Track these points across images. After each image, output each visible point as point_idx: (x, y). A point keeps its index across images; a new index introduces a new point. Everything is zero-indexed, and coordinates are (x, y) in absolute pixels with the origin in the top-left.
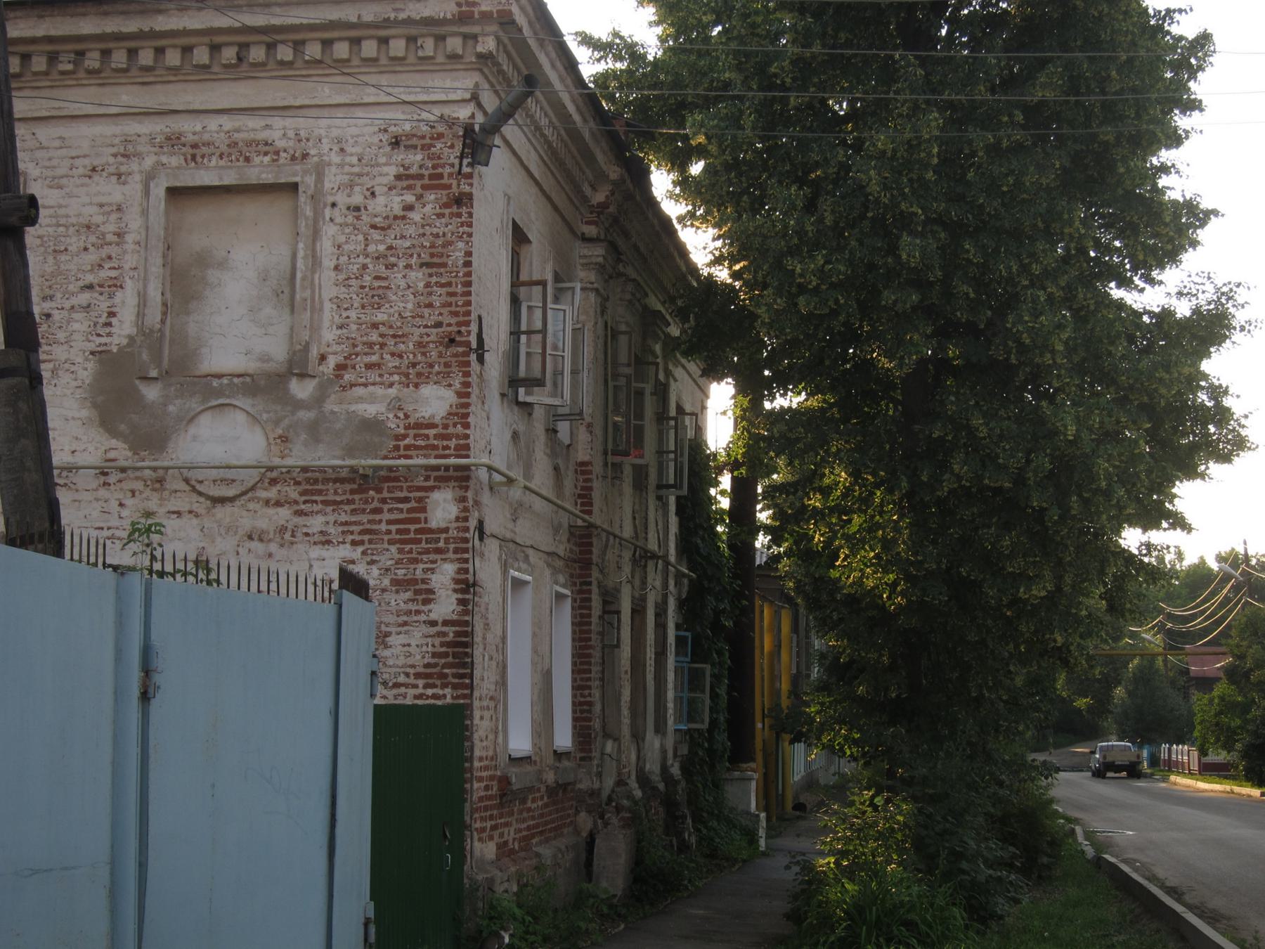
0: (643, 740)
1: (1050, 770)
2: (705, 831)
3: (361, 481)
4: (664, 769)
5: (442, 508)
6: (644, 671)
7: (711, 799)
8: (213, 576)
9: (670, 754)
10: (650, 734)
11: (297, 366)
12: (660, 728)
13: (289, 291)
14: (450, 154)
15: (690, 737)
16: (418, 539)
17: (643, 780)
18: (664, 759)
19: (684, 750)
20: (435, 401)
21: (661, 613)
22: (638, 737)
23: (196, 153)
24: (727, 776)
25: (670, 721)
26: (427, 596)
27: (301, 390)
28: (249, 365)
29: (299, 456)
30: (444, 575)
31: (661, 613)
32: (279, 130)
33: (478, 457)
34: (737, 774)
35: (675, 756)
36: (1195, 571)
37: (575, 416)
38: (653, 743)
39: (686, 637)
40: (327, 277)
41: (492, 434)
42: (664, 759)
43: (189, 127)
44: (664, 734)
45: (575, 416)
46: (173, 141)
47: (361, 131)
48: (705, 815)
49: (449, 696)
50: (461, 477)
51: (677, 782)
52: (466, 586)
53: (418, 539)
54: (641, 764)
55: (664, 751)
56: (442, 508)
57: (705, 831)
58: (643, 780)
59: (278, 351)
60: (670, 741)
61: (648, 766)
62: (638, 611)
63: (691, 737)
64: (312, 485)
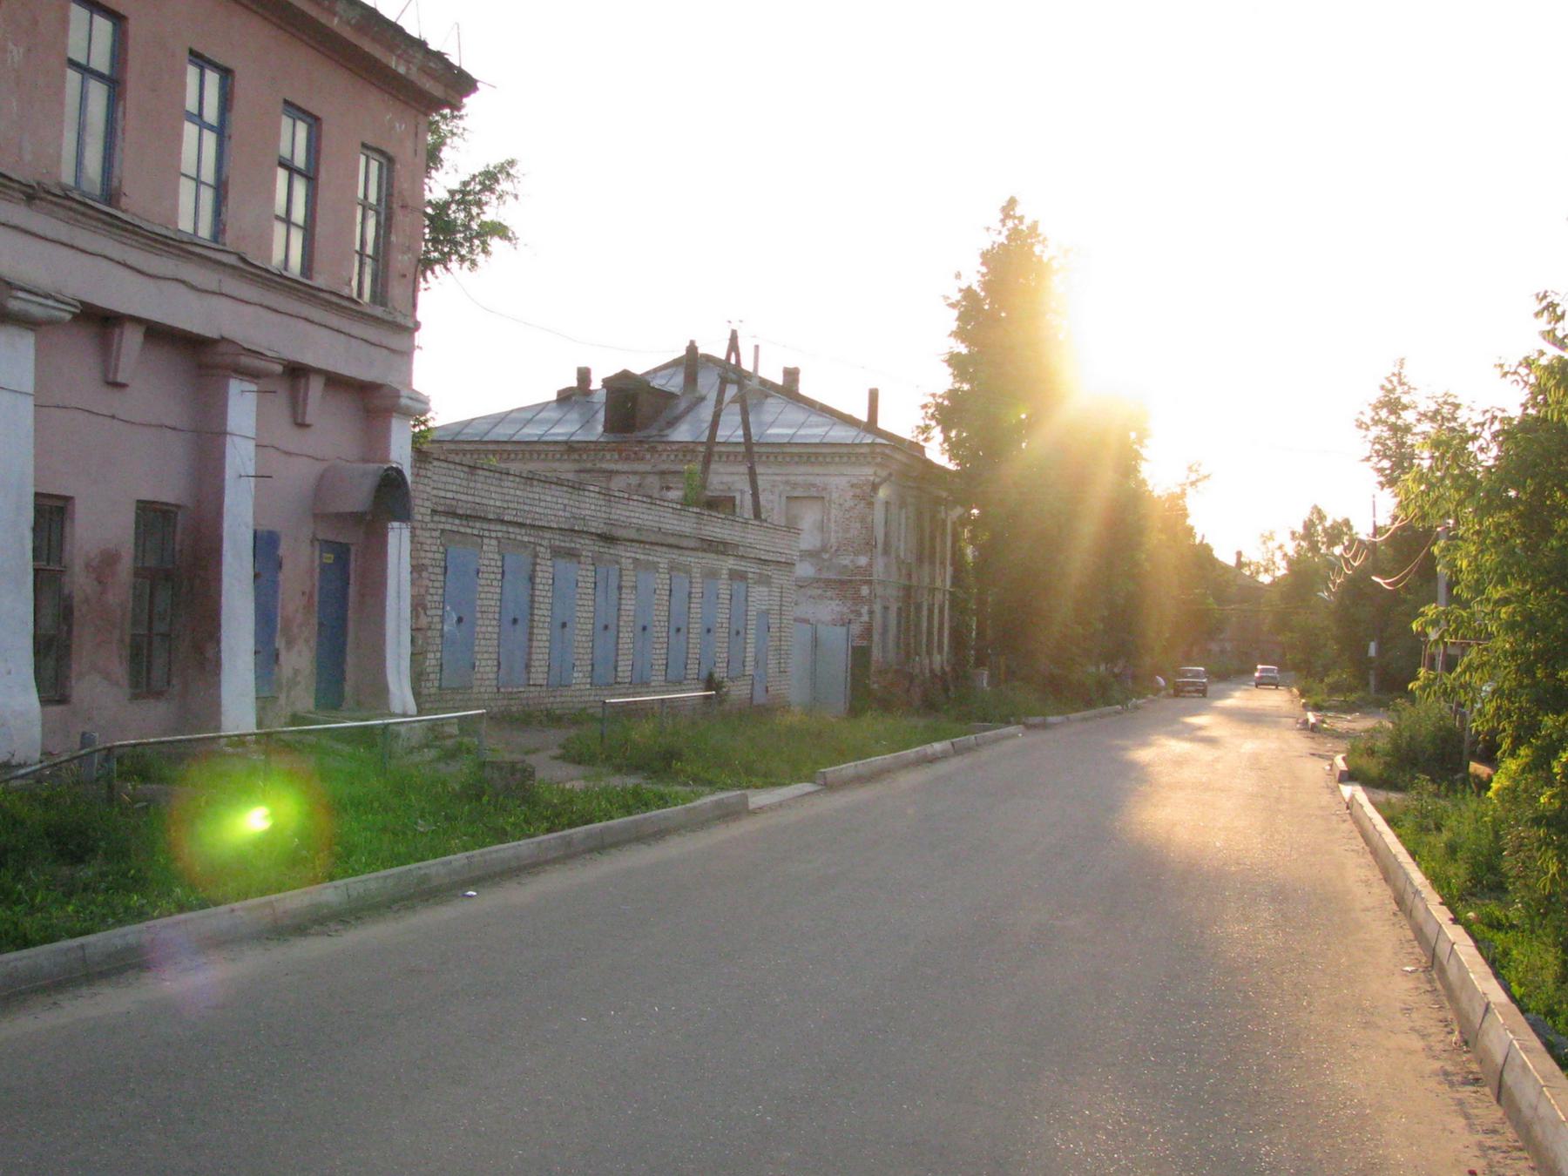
1: (1125, 749)
3: (842, 582)
5: (865, 591)
8: (731, 391)
10: (935, 651)
11: (824, 549)
13: (822, 527)
14: (867, 489)
16: (858, 599)
17: (932, 671)
20: (863, 561)
21: (941, 611)
22: (929, 653)
23: (795, 485)
26: (860, 615)
27: (826, 556)
28: (809, 547)
29: (825, 575)
30: (865, 610)
31: (941, 611)
32: (818, 480)
33: (875, 577)
38: (937, 658)
40: (833, 525)
41: (879, 570)
43: (792, 478)
46: (787, 483)
47: (843, 482)
49: (865, 643)
50: (870, 583)
52: (871, 612)
53: (858, 599)
56: (865, 591)
58: (932, 671)
59: (818, 544)
62: (931, 611)
64: (828, 583)
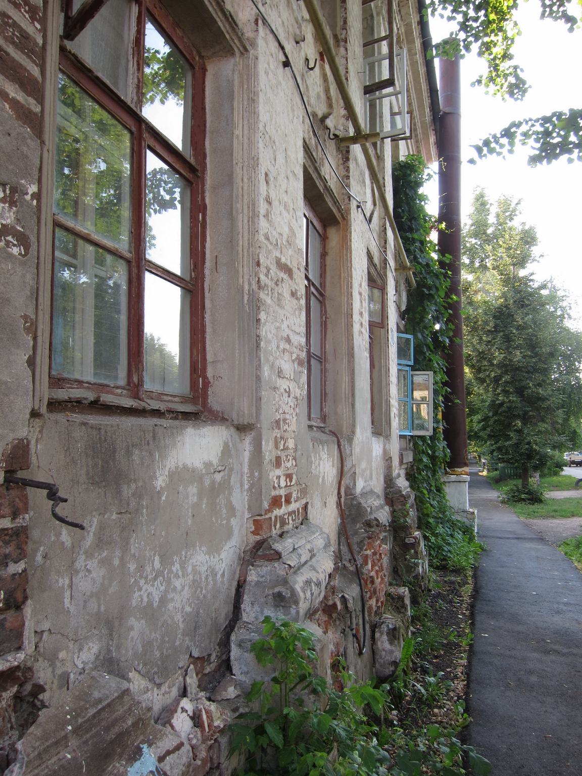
0: (350, 440)
2: (433, 539)
4: (389, 482)
6: (349, 326)
7: (435, 503)
9: (396, 462)
10: (363, 431)
12: (380, 428)
15: (414, 443)
18: (389, 468)
19: (409, 457)
24: (445, 479)
25: (395, 423)
34: (453, 478)
35: (401, 463)
36: (419, 210)
37: (318, 584)
39: (408, 340)
42: (389, 468)
44: (388, 437)
45: (318, 584)
48: (431, 520)
51: (405, 498)
54: (346, 481)
55: (388, 459)
57: (433, 539)
60: (395, 446)
61: (360, 485)
63: (415, 444)
